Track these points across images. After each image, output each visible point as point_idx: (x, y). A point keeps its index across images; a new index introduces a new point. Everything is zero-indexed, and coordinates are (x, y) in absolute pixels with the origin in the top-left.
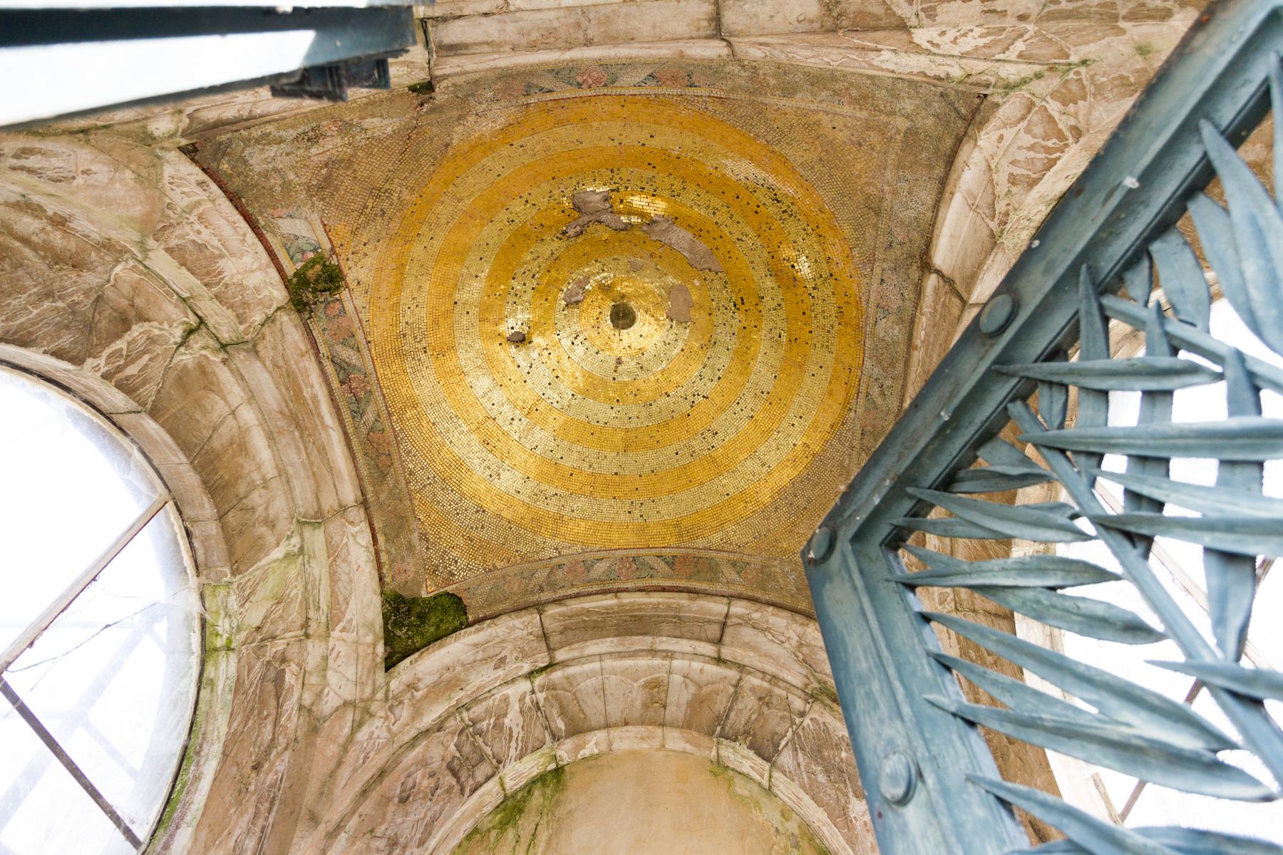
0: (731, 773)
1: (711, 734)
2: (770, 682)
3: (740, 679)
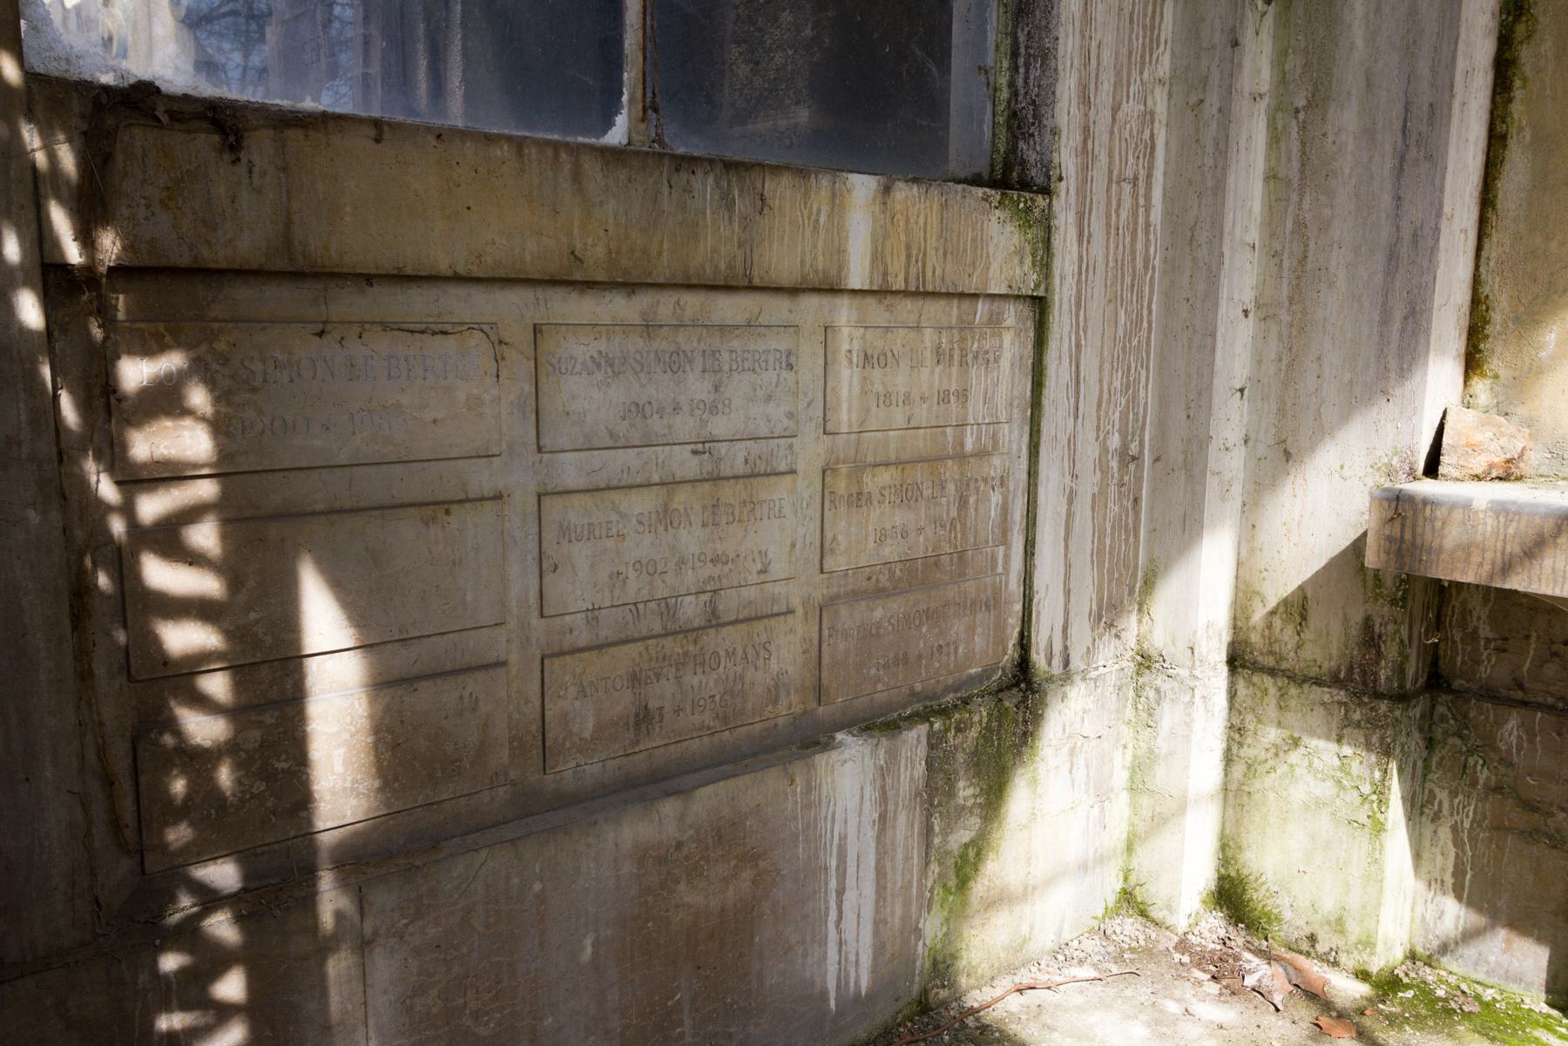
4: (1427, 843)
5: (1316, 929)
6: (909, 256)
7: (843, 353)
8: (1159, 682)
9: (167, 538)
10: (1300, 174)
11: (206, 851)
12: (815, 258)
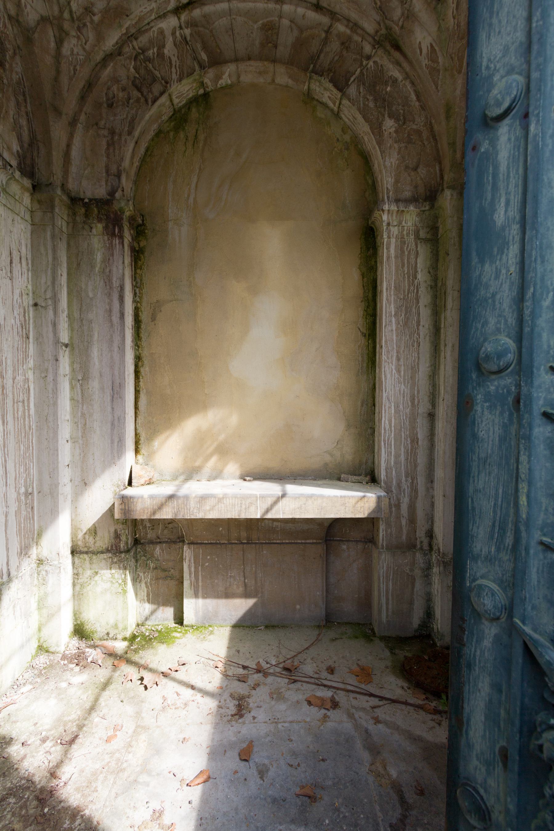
0: (315, 102)
1: (306, 70)
2: (351, 29)
3: (331, 26)
4: (138, 590)
5: (109, 630)
8: (46, 568)
10: (81, 399)
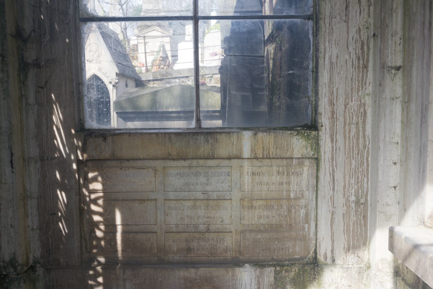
6: (263, 150)
7: (245, 173)
9: (95, 202)
11: (99, 254)
12: (233, 151)
